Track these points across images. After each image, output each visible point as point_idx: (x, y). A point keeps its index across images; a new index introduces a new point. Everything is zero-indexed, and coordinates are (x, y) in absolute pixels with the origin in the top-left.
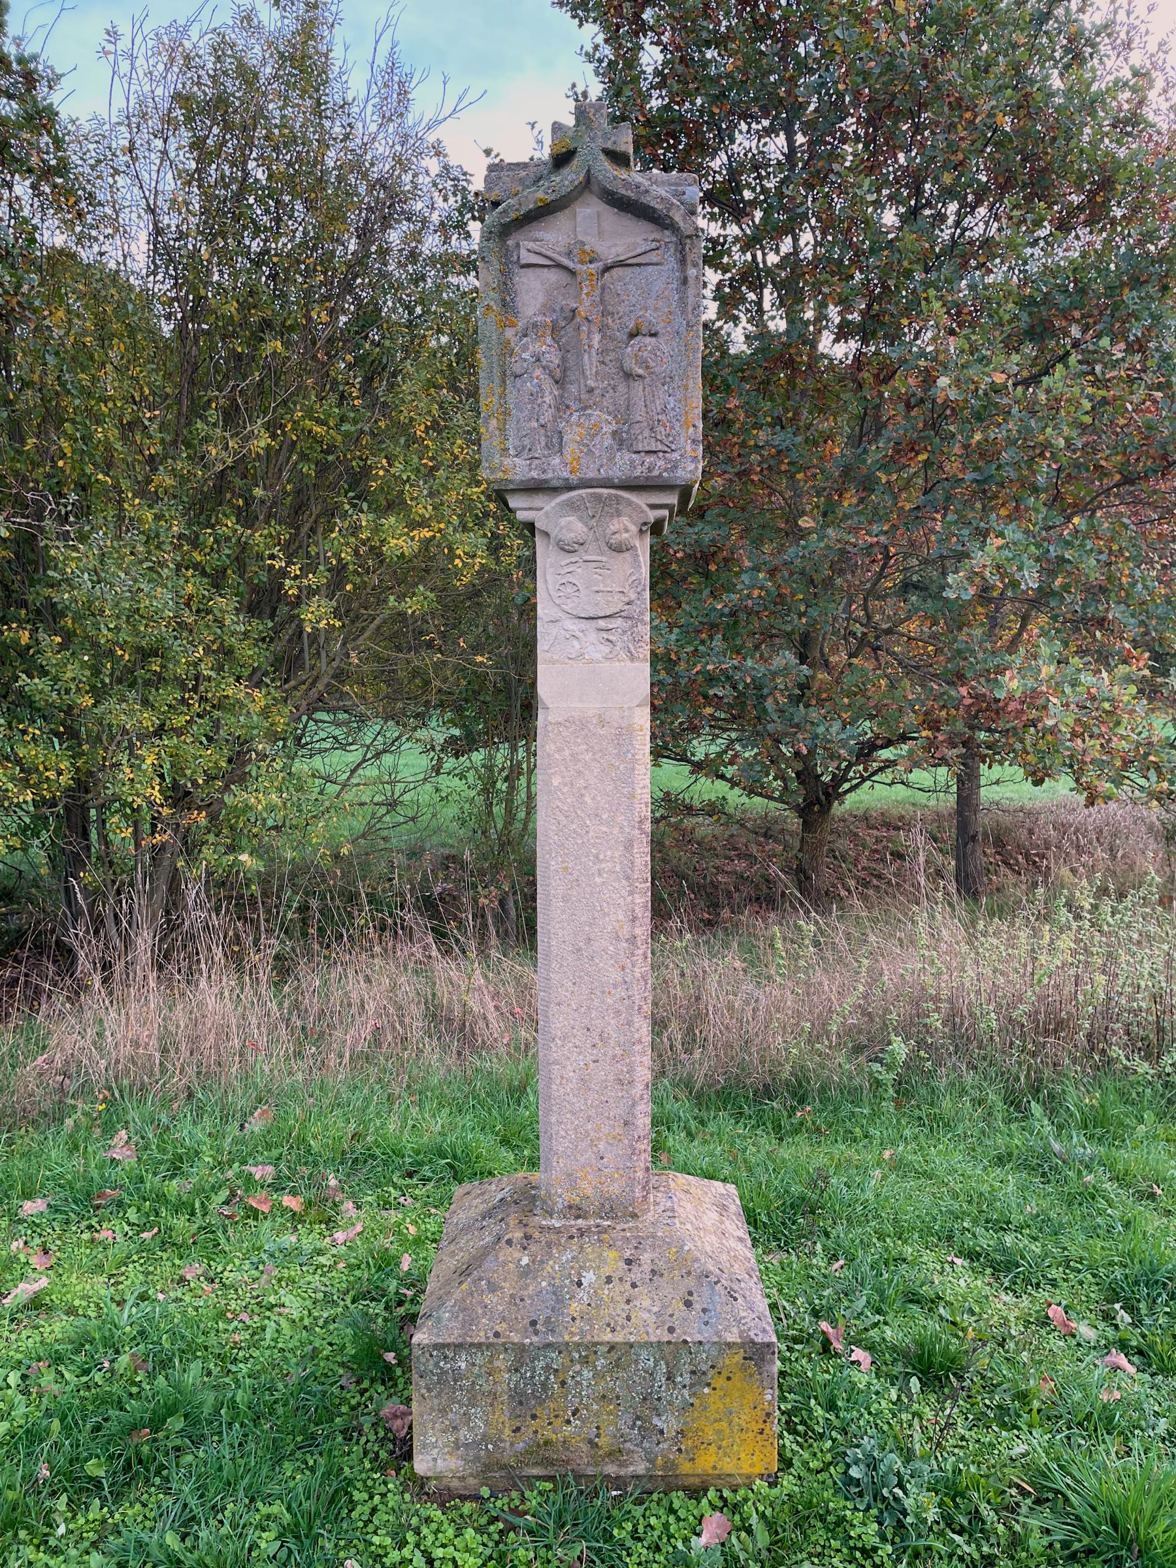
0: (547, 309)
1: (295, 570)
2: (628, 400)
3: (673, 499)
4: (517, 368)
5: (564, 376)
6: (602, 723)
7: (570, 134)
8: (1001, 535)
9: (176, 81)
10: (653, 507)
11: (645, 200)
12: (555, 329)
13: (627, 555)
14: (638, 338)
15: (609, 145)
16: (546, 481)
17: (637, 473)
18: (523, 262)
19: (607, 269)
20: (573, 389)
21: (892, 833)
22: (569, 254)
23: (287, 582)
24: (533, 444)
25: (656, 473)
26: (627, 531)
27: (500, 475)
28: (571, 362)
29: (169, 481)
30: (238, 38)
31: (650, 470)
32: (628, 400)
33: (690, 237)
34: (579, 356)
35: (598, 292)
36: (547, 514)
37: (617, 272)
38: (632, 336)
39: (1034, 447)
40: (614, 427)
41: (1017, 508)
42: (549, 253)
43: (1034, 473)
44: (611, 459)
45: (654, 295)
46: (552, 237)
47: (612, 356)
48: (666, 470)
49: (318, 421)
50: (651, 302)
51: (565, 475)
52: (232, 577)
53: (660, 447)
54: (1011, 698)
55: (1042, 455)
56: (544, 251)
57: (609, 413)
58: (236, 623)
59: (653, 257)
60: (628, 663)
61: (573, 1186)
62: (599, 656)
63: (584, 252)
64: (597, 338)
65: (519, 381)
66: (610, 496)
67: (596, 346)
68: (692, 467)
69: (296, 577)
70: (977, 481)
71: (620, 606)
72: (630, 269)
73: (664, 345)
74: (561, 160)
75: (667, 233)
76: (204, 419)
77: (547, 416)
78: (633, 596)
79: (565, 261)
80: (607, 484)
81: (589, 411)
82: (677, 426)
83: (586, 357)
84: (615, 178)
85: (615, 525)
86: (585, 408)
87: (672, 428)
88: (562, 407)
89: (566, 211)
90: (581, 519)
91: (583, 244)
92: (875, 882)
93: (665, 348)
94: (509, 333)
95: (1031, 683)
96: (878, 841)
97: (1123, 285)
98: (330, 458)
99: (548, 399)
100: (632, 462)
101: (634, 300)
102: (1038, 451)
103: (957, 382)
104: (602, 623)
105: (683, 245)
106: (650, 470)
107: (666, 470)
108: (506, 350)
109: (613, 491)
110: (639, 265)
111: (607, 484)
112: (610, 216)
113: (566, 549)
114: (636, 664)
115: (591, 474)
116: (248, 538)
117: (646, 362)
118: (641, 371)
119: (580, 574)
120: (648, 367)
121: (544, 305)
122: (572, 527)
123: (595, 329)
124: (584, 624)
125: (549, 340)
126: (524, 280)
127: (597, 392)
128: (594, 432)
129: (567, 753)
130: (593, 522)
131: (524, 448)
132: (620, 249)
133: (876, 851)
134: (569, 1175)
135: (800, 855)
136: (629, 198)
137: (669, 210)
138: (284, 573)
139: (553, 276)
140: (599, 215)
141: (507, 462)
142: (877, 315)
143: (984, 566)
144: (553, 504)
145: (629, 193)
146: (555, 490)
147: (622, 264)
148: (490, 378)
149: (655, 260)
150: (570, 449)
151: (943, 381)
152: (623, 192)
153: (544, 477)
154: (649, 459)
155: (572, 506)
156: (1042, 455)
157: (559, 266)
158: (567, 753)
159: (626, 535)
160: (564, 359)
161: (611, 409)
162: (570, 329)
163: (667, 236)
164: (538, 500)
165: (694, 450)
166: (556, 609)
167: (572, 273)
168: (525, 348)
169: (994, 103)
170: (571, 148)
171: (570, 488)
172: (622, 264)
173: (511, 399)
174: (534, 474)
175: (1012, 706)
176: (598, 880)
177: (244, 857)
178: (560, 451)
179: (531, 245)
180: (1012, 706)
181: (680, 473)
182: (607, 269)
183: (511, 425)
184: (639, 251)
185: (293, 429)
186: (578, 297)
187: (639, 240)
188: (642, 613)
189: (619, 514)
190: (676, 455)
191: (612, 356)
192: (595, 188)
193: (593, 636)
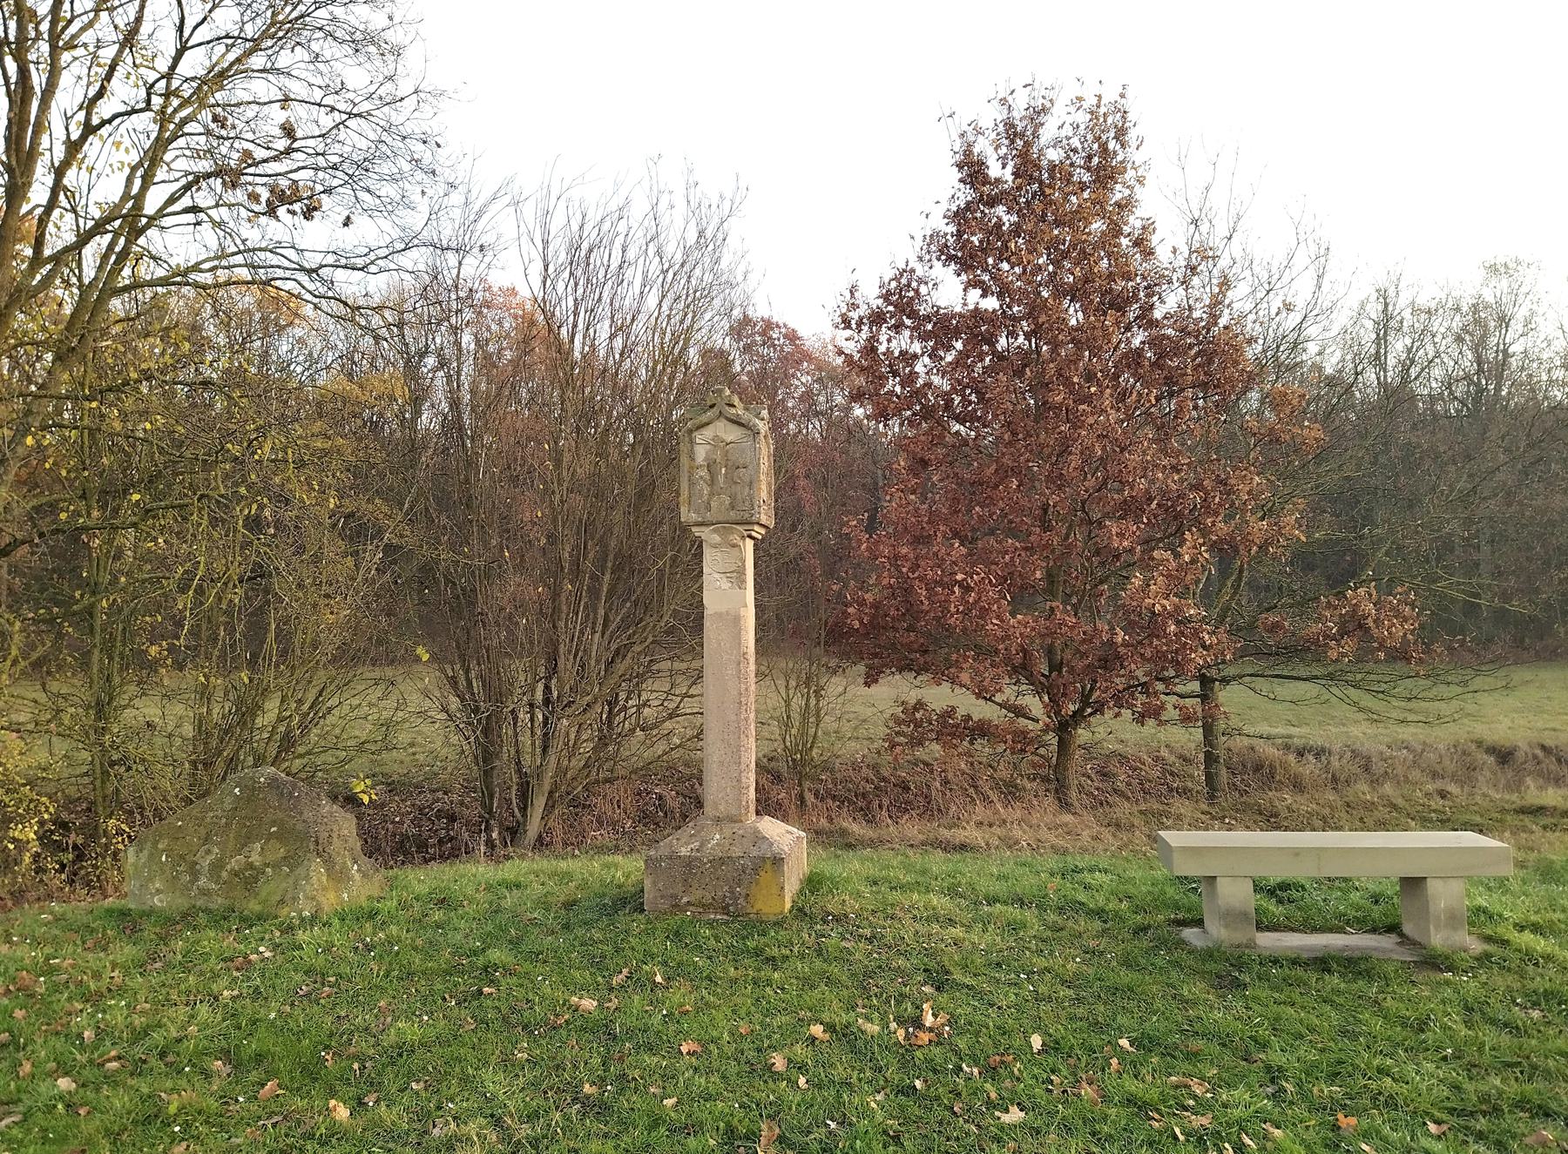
88: (712, 494)
122: (717, 538)
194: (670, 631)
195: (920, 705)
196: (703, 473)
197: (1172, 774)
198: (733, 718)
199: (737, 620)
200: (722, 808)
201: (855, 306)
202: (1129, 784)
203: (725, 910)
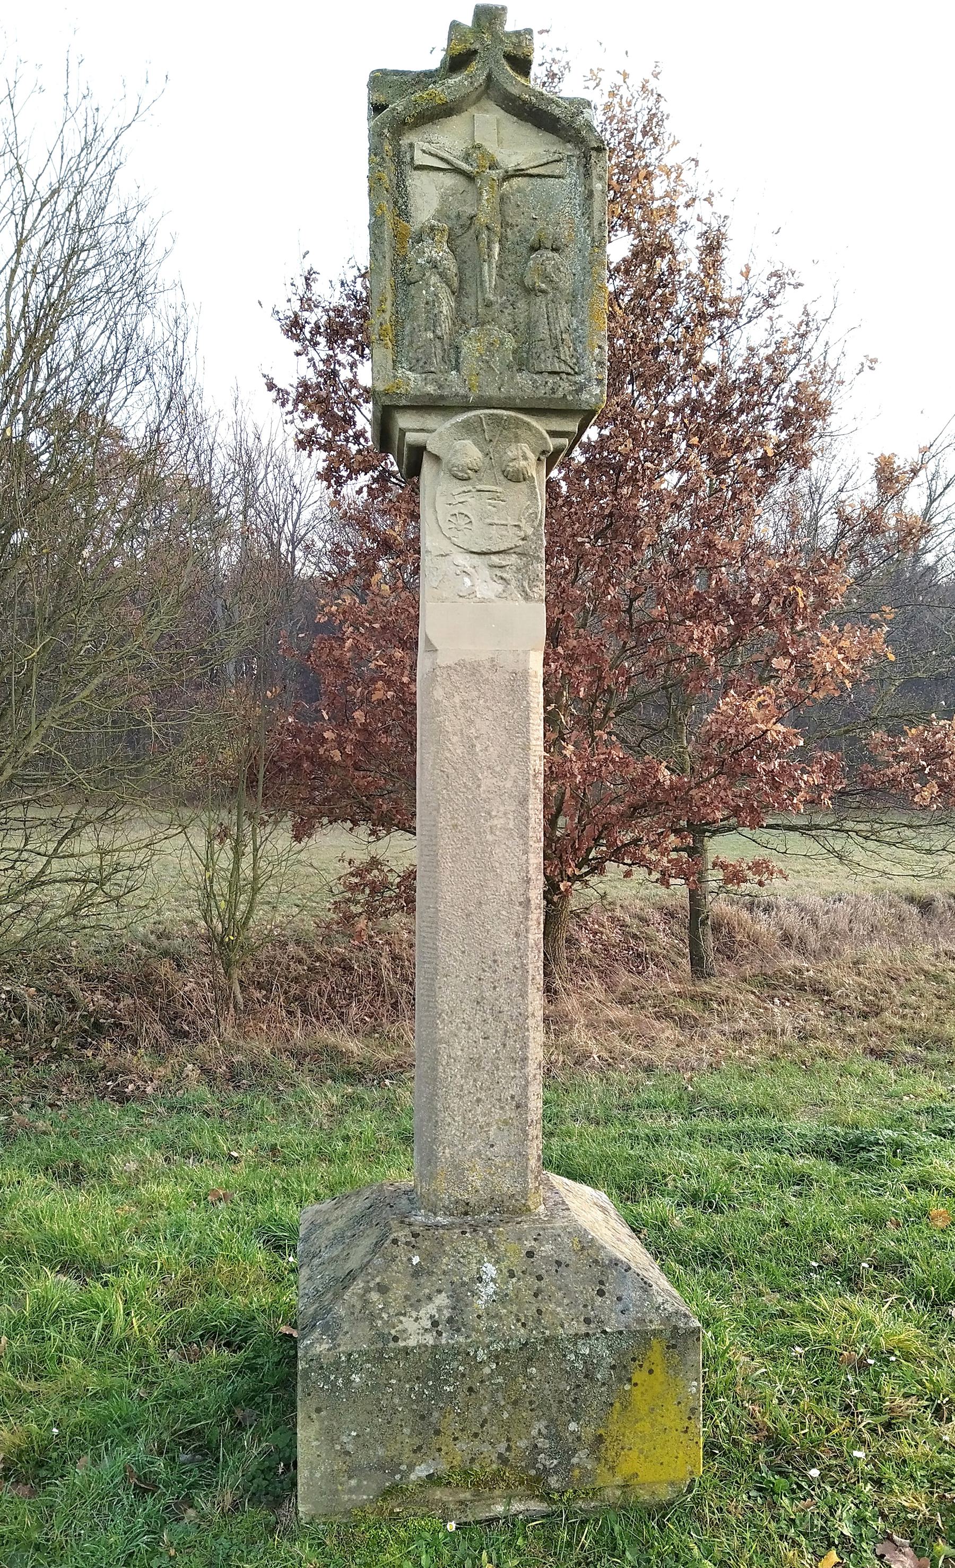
0: (441, 214)
5: (461, 288)
6: (494, 667)
10: (554, 434)
13: (523, 486)
16: (442, 397)
18: (417, 163)
22: (467, 157)
25: (560, 394)
31: (553, 391)
36: (440, 434)
37: (515, 182)
38: (533, 249)
42: (446, 155)
46: (448, 139)
53: (564, 368)
59: (556, 169)
60: (523, 602)
61: (461, 1181)
72: (533, 180)
74: (457, 62)
75: (569, 146)
77: (445, 328)
83: (486, 267)
88: (459, 320)
104: (495, 559)
105: (587, 157)
106: (553, 391)
107: (570, 393)
109: (512, 414)
114: (532, 604)
115: (491, 391)
119: (473, 504)
122: (470, 452)
124: (476, 560)
129: (457, 699)
134: (456, 1167)
139: (449, 180)
144: (448, 424)
149: (557, 172)
155: (468, 428)
157: (457, 171)
158: (457, 699)
159: (523, 463)
163: (569, 149)
164: (431, 421)
166: (447, 542)
171: (468, 408)
174: (430, 389)
176: (490, 838)
179: (426, 146)
182: (508, 177)
189: (517, 439)
190: (580, 379)
193: (486, 573)
194: (45, 759)
195: (375, 863)
196: (438, 251)
197: (635, 936)
198: (508, 941)
199: (525, 675)
200: (476, 1179)
201: (307, 303)
202: (594, 951)
203: (535, 1485)
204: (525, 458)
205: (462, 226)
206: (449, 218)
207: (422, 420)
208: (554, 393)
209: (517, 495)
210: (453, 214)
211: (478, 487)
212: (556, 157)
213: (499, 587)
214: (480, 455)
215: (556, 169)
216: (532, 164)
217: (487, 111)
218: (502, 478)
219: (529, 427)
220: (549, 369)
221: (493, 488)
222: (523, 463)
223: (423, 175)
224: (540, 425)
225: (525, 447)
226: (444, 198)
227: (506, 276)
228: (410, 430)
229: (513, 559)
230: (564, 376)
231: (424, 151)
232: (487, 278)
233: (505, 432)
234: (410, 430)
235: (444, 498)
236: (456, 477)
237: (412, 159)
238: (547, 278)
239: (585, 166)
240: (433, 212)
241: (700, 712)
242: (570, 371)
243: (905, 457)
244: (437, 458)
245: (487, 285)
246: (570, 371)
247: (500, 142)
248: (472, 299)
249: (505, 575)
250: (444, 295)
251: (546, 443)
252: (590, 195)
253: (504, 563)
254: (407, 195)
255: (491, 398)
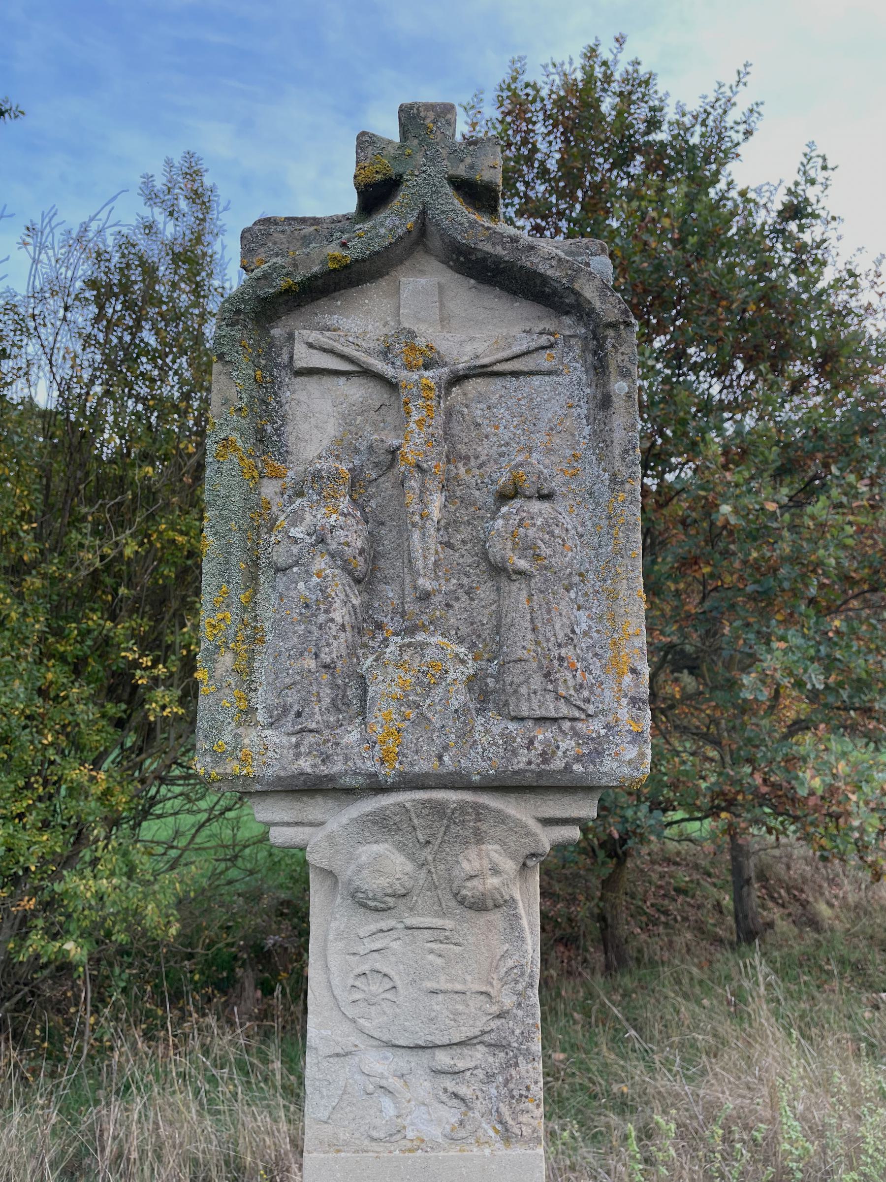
0: (342, 447)
1: (146, 661)
2: (499, 615)
3: (588, 809)
4: (280, 556)
7: (391, 150)
8: (783, 639)
9: (85, 270)
11: (526, 261)
12: (356, 483)
13: (496, 917)
14: (517, 503)
15: (461, 171)
16: (331, 778)
17: (520, 762)
18: (299, 364)
19: (457, 379)
20: (390, 592)
21: (673, 868)
22: (385, 353)
23: (138, 673)
24: (305, 702)
25: (558, 764)
26: (496, 871)
27: (232, 767)
28: (387, 544)
29: (38, 583)
30: (143, 243)
31: (546, 757)
32: (499, 615)
33: (610, 325)
34: (403, 533)
35: (440, 419)
37: (473, 386)
38: (504, 497)
39: (808, 565)
40: (471, 668)
41: (791, 615)
43: (807, 586)
44: (465, 734)
45: (543, 426)
46: (359, 323)
47: (465, 533)
48: (578, 759)
49: (182, 533)
50: (538, 439)
51: (370, 766)
52: (93, 665)
53: (565, 710)
54: (812, 793)
55: (814, 571)
56: (339, 347)
57: (461, 640)
58: (87, 712)
59: (543, 361)
62: (436, 1132)
63: (413, 349)
64: (436, 501)
65: (282, 581)
66: (462, 807)
67: (436, 514)
68: (631, 753)
69: (147, 668)
70: (758, 592)
71: (481, 1023)
72: (499, 382)
73: (566, 515)
75: (567, 320)
76: (79, 530)
77: (336, 648)
78: (508, 1001)
79: (378, 365)
80: (456, 781)
81: (420, 637)
82: (596, 666)
83: (416, 536)
84: (473, 224)
85: (470, 861)
86: (412, 631)
87: (587, 670)
88: (367, 626)
89: (383, 282)
90: (401, 848)
91: (412, 334)
92: (663, 919)
93: (567, 521)
94: (269, 489)
95: (828, 779)
96: (662, 877)
97: (855, 433)
98: (189, 562)
99: (339, 614)
100: (508, 739)
101: (506, 436)
102: (811, 568)
103: (736, 511)
104: (443, 1059)
106: (546, 757)
107: (578, 759)
108: (260, 520)
110: (515, 374)
111: (456, 781)
112: (463, 295)
113: (366, 903)
114: (518, 1151)
115: (424, 766)
116: (109, 630)
117: (533, 546)
118: (523, 564)
119: (398, 953)
120: (537, 557)
121: (338, 441)
122: (385, 862)
123: (433, 484)
125: (344, 504)
126: (301, 396)
127: (437, 599)
128: (430, 679)
130: (427, 854)
131: (286, 710)
132: (480, 347)
133: (661, 887)
135: (601, 904)
136: (498, 260)
137: (572, 279)
138: (136, 664)
139: (356, 391)
140: (441, 287)
141: (251, 738)
142: (659, 454)
143: (775, 670)
145: (499, 250)
146: (350, 793)
147: (484, 372)
148: (224, 573)
149: (546, 365)
150: (383, 714)
151: (726, 509)
152: (488, 248)
153: (324, 770)
154: (542, 735)
155: (382, 824)
156: (814, 571)
157: (367, 373)
159: (493, 881)
160: (372, 538)
161: (465, 630)
162: (386, 484)
163: (568, 325)
164: (315, 809)
165: (635, 720)
166: (346, 1027)
167: (392, 385)
168: (296, 519)
169: (747, 293)
170: (392, 173)
171: (377, 787)
172: (484, 372)
173: (267, 612)
174: (305, 765)
175: (812, 801)
177: (69, 946)
178: (363, 712)
179: (314, 336)
180: (812, 801)
181: (608, 765)
182: (457, 379)
183: (263, 664)
184: (516, 349)
185: (158, 538)
186: (401, 427)
187: (516, 331)
188: (526, 1037)
189: (479, 838)
190: (596, 727)
191: (465, 533)
192: (435, 242)
193: (424, 1086)
204: (496, 871)
205: (377, 465)
206: (357, 451)
207: (298, 806)
208: (545, 761)
209: (482, 938)
210: (363, 446)
211: (409, 921)
212: (544, 340)
213: (451, 1115)
214: (409, 867)
215: (543, 361)
216: (500, 355)
217: (422, 272)
218: (453, 903)
219: (502, 818)
220: (538, 713)
221: (438, 922)
222: (493, 881)
223: (312, 384)
224: (520, 811)
225: (492, 850)
226: (346, 420)
227: (458, 544)
228: (276, 824)
229: (479, 1055)
230: (566, 725)
231: (311, 346)
232: (418, 554)
233: (454, 829)
234: (276, 824)
235: (340, 945)
236: (365, 906)
237: (291, 358)
238: (529, 549)
239: (595, 353)
240: (326, 443)
241: (774, 410)
242: (577, 714)
243: (618, 35)
244: (330, 874)
245: (420, 564)
246: (577, 714)
247: (444, 320)
248: (396, 586)
249: (463, 1090)
250: (340, 587)
251: (537, 842)
252: (605, 402)
253: (461, 1065)
254: (284, 418)
255: (426, 775)
